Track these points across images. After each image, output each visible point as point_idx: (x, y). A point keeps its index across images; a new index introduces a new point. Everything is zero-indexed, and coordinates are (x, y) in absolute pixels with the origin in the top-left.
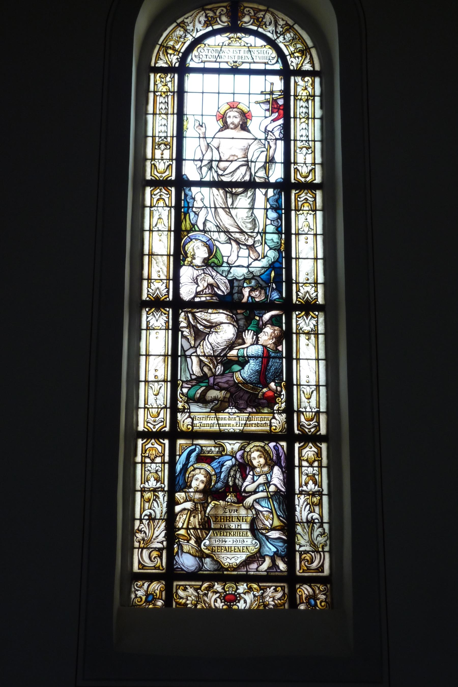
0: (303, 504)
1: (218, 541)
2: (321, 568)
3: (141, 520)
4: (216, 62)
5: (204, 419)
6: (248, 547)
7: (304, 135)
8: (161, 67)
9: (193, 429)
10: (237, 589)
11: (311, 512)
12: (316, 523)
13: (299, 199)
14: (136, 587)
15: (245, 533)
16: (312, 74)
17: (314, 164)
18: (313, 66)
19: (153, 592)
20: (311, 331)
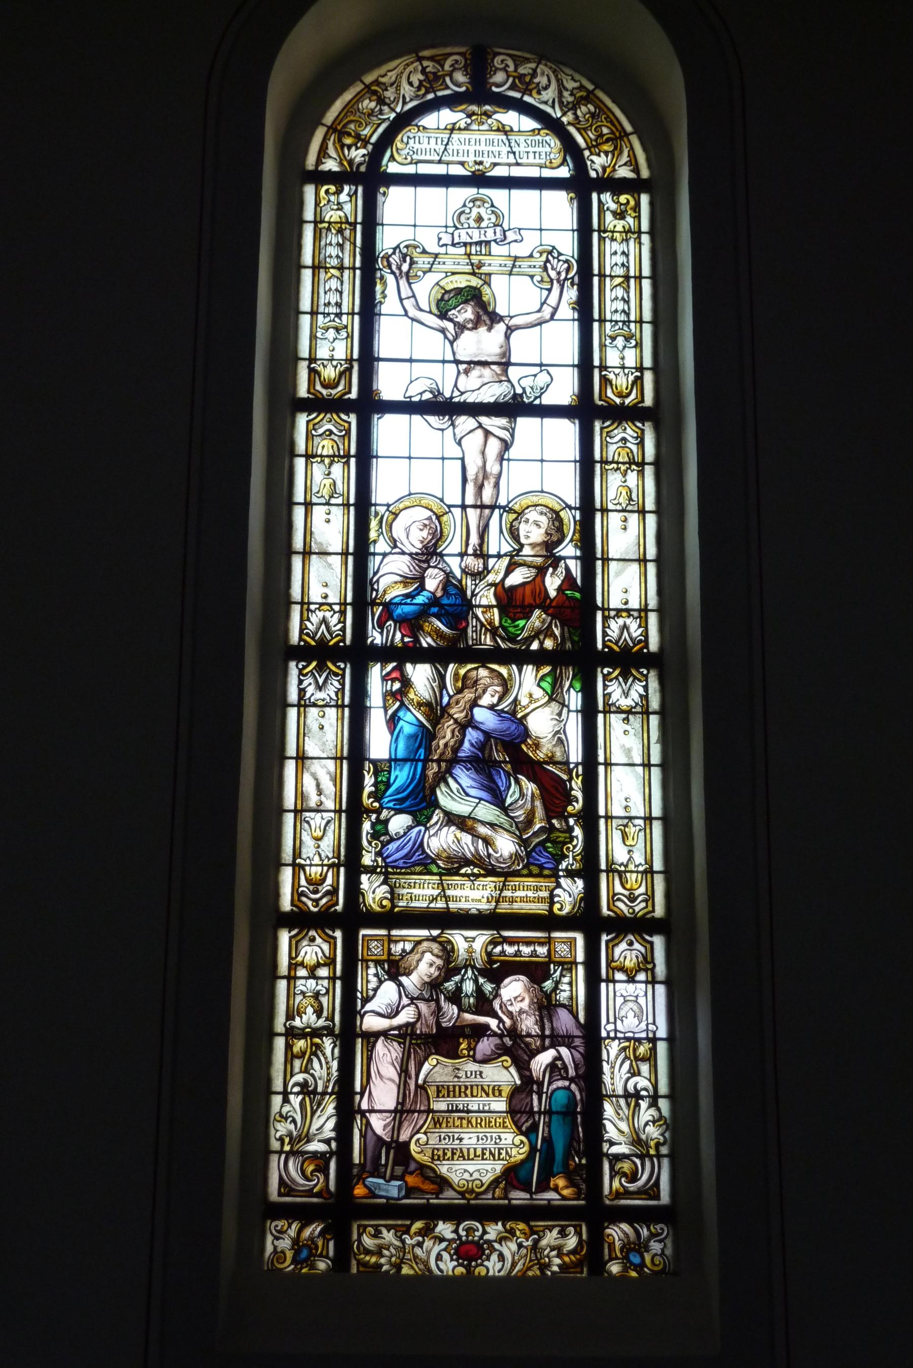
0: (617, 1058)
1: (482, 1139)
2: (652, 1191)
3: (285, 1094)
4: (440, 162)
5: (417, 886)
6: (509, 1150)
7: (333, 301)
8: (624, 180)
9: (394, 906)
10: (485, 1232)
11: (634, 1075)
12: (642, 1098)
13: (313, 432)
14: (274, 1232)
15: (501, 1120)
16: (633, 186)
17: (641, 369)
18: (636, 170)
19: (310, 1243)
20: (635, 707)
